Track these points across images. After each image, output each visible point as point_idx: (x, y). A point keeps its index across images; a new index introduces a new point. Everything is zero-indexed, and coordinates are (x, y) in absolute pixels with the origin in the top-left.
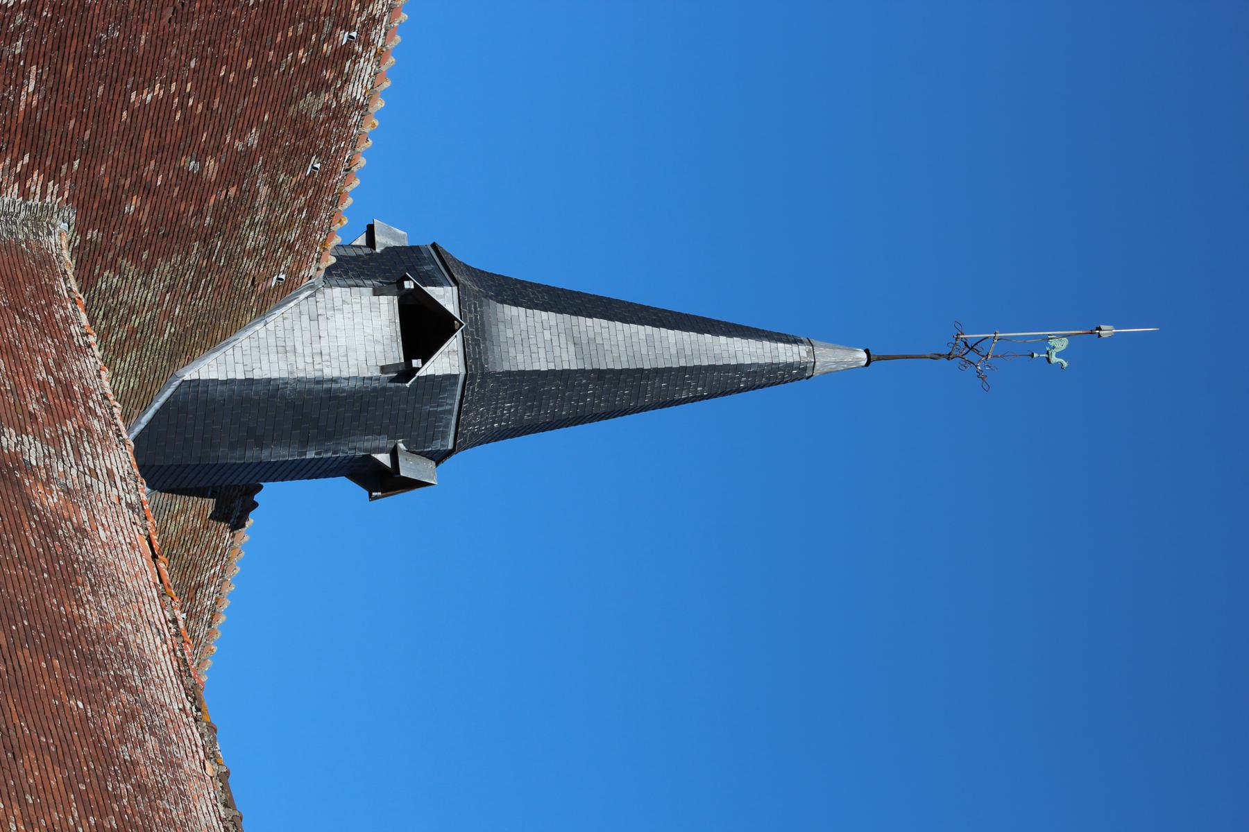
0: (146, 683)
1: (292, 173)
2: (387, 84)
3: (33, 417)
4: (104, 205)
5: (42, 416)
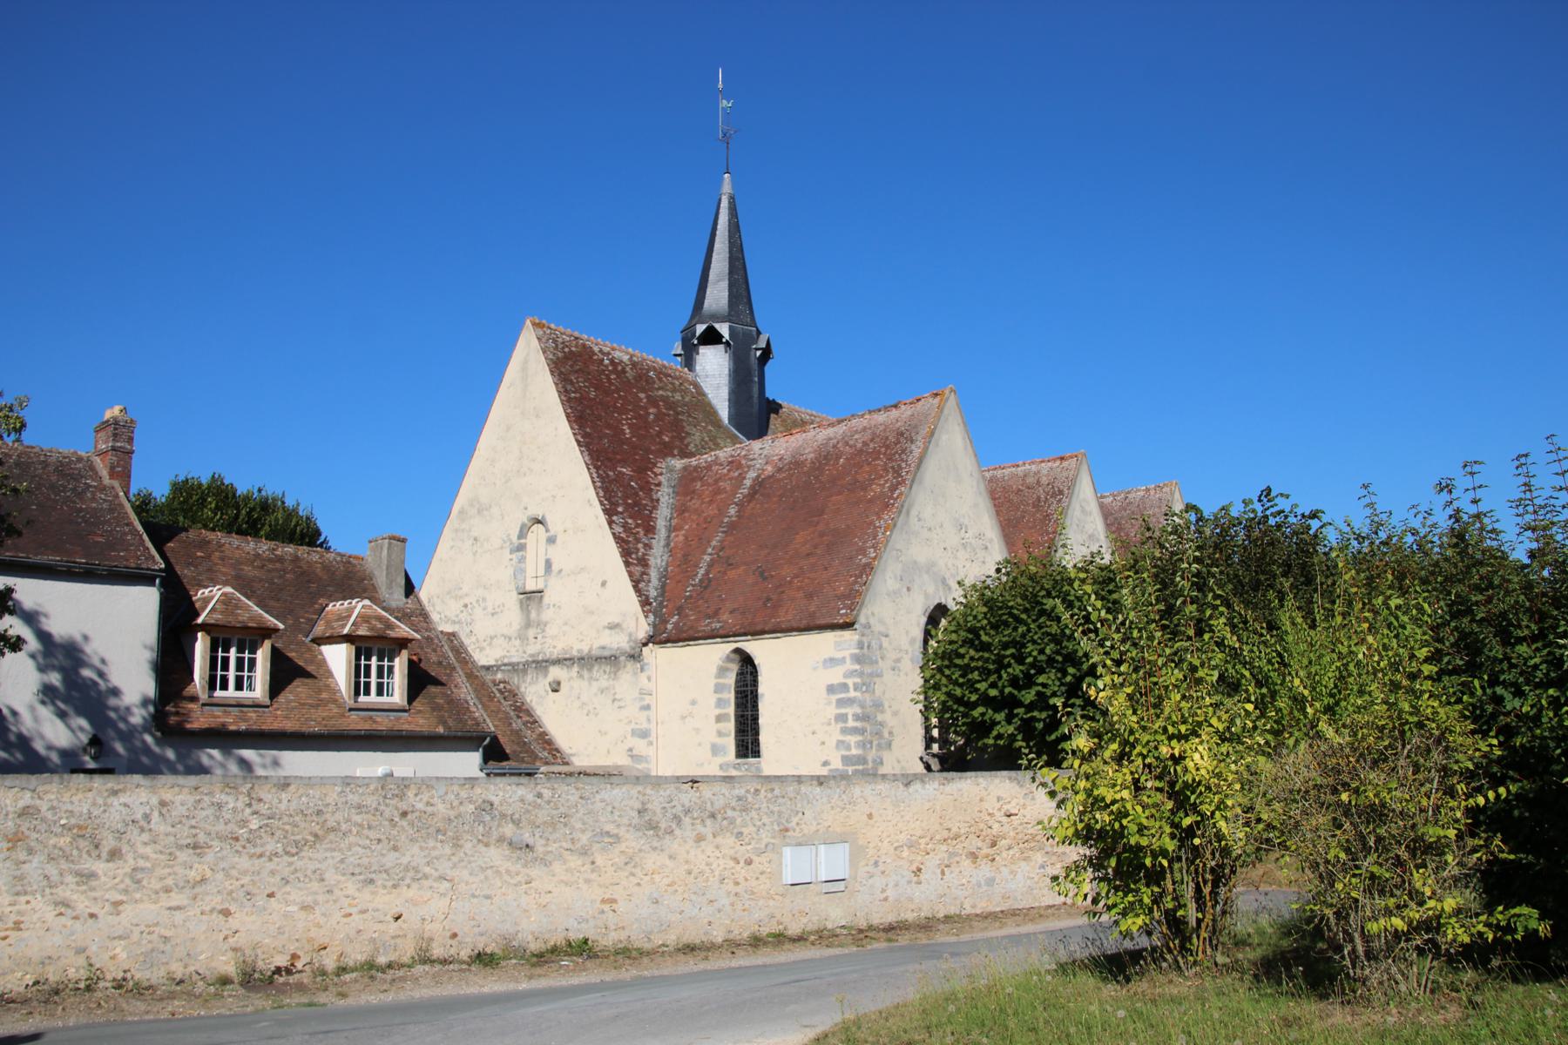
0: (835, 438)
1: (654, 382)
2: (623, 347)
3: (740, 474)
4: (665, 447)
5: (740, 471)
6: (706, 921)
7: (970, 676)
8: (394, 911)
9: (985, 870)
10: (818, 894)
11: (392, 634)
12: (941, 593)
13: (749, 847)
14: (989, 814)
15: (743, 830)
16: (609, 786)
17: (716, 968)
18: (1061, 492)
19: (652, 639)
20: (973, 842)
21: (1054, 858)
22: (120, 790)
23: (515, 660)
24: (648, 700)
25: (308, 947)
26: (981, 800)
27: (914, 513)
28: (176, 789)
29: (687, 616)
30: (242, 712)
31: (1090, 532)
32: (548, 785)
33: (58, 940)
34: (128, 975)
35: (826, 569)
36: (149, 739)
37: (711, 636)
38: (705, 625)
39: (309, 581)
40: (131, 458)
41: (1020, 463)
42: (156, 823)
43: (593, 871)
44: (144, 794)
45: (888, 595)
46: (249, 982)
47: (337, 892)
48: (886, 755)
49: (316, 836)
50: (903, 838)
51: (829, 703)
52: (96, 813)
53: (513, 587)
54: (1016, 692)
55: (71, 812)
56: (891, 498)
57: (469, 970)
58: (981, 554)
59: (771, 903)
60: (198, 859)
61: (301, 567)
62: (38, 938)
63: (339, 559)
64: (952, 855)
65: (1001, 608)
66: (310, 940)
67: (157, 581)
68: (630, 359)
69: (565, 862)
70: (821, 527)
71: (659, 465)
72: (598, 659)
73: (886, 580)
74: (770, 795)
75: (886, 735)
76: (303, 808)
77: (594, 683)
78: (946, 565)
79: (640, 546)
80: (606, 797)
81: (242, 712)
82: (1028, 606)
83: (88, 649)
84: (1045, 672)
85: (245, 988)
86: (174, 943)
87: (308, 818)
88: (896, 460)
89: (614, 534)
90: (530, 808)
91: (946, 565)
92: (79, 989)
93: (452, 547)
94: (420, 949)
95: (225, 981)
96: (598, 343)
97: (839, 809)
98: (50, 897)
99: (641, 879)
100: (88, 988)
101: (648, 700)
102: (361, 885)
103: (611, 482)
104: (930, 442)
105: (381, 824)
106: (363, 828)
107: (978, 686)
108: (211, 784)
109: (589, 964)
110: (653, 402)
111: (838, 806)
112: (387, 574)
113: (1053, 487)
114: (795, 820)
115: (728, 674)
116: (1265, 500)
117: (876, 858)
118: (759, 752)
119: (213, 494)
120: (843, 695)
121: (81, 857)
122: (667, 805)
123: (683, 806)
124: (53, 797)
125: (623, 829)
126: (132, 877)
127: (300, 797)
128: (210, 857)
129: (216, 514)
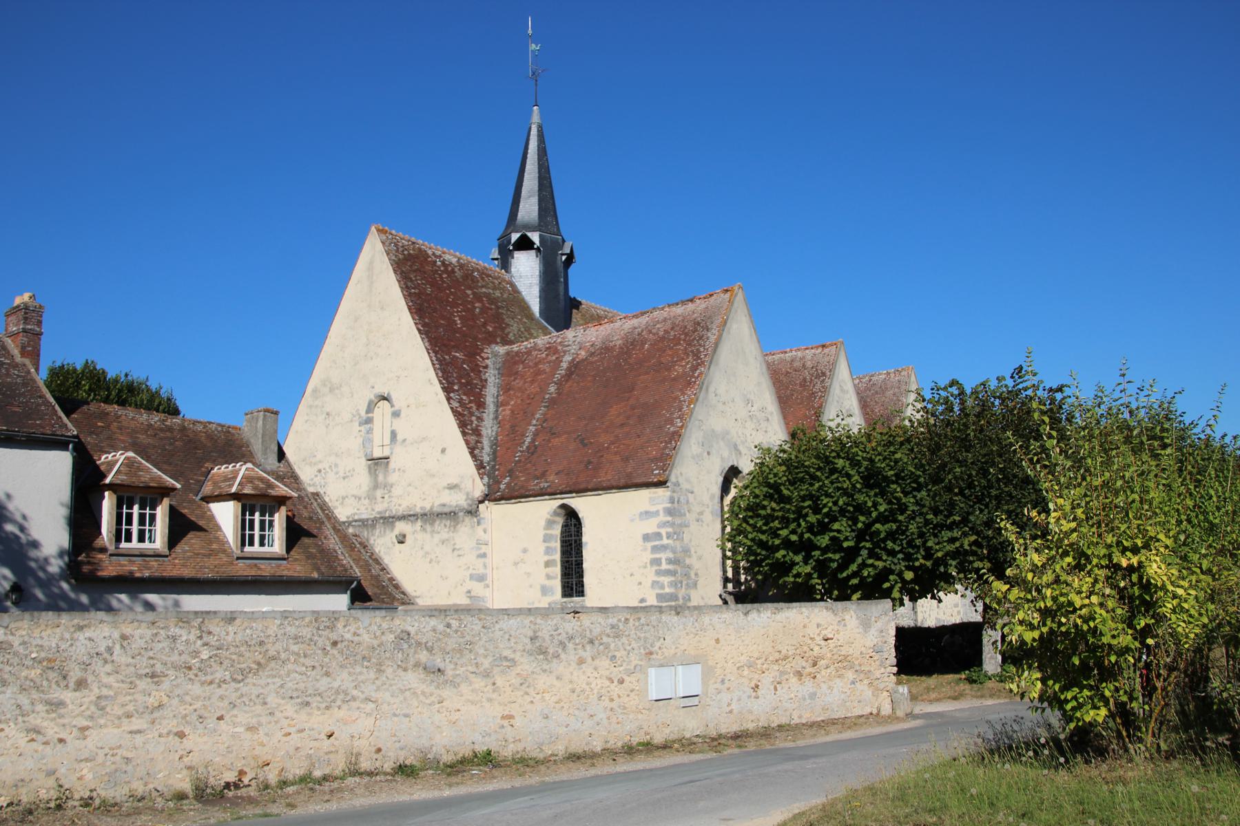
1: (478, 281)
2: (452, 251)
3: (557, 358)
6: (587, 733)
7: (772, 525)
8: (328, 729)
9: (809, 686)
10: (677, 708)
11: (273, 492)
12: (734, 456)
13: (621, 669)
14: (811, 638)
15: (616, 653)
16: (506, 617)
17: (605, 773)
18: (824, 374)
19: (488, 497)
20: (799, 662)
21: (862, 676)
22: (86, 626)
23: (364, 517)
24: (484, 549)
25: (253, 763)
26: (804, 627)
27: (712, 389)
28: (136, 624)
29: (518, 477)
30: (145, 561)
31: (847, 407)
32: (456, 617)
33: (30, 764)
34: (94, 794)
35: (639, 436)
36: (65, 585)
37: (541, 493)
38: (534, 485)
39: (196, 448)
40: (40, 339)
41: (788, 350)
42: (118, 655)
43: (494, 691)
44: (106, 629)
45: (693, 457)
46: (202, 797)
47: (278, 714)
48: (693, 593)
49: (259, 664)
50: (744, 659)
51: (645, 550)
52: (63, 647)
53: (362, 454)
54: (812, 537)
55: (42, 646)
56: (693, 376)
57: (395, 780)
58: (764, 424)
59: (640, 716)
60: (155, 687)
61: (188, 436)
62: (12, 762)
63: (220, 429)
64: (782, 673)
65: (797, 468)
66: (255, 758)
67: (71, 446)
68: (458, 261)
69: (471, 683)
70: (632, 402)
71: (485, 351)
72: (439, 515)
73: (690, 446)
74: (637, 624)
75: (693, 576)
76: (247, 639)
77: (435, 535)
78: (737, 433)
79: (474, 418)
80: (504, 626)
81: (145, 561)
82: (821, 465)
83: (11, 506)
84: (837, 521)
85: (200, 803)
86: (134, 763)
87: (252, 649)
88: (695, 345)
89: (452, 408)
90: (441, 637)
91: (737, 433)
92: (50, 808)
93: (306, 421)
94: (350, 763)
95: (181, 796)
96: (432, 248)
97: (692, 635)
98: (22, 724)
99: (534, 698)
100: (59, 807)
101: (484, 549)
102: (299, 707)
103: (447, 364)
104: (723, 330)
105: (315, 653)
106: (300, 657)
107: (780, 532)
108: (167, 619)
109: (496, 772)
110: (478, 297)
111: (692, 633)
112: (263, 442)
113: (817, 370)
114: (658, 644)
115: (555, 526)
116: (1017, 377)
117: (722, 676)
118: (583, 592)
119: (87, 378)
120: (657, 543)
121: (50, 687)
122: (554, 633)
123: (567, 634)
124: (24, 633)
125: (518, 654)
126: (96, 705)
127: (245, 630)
128: (166, 685)
129: (90, 395)
